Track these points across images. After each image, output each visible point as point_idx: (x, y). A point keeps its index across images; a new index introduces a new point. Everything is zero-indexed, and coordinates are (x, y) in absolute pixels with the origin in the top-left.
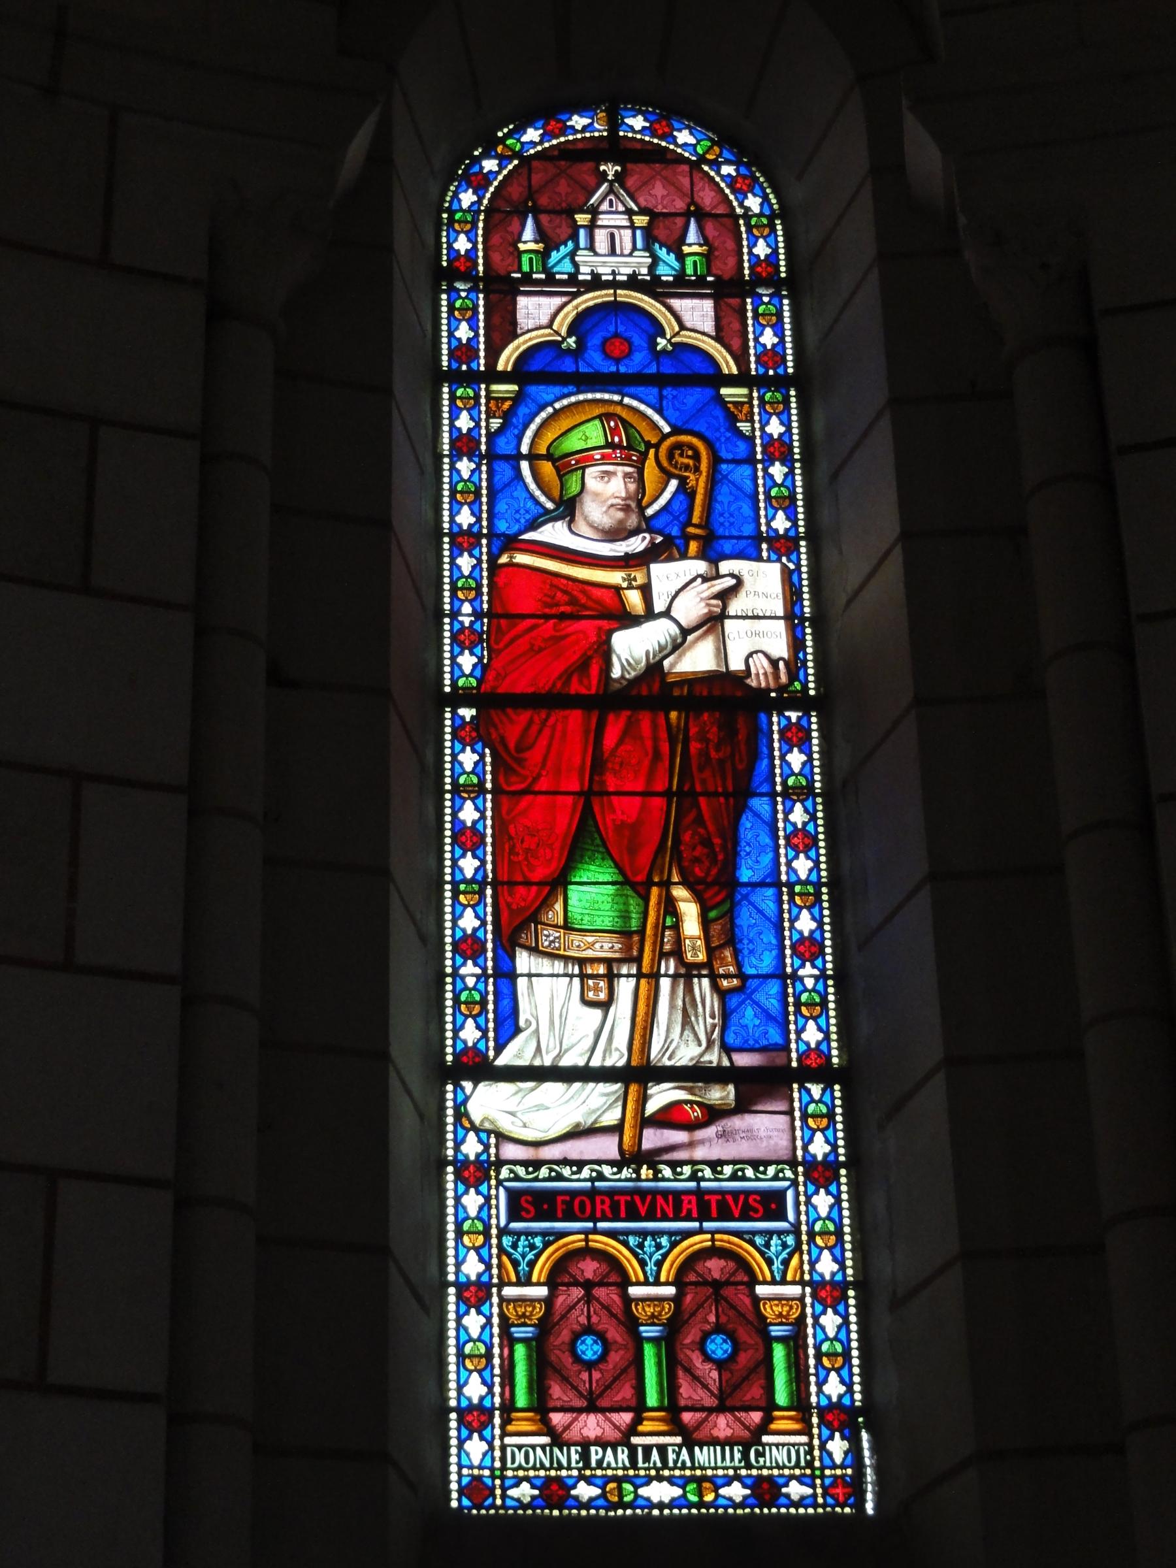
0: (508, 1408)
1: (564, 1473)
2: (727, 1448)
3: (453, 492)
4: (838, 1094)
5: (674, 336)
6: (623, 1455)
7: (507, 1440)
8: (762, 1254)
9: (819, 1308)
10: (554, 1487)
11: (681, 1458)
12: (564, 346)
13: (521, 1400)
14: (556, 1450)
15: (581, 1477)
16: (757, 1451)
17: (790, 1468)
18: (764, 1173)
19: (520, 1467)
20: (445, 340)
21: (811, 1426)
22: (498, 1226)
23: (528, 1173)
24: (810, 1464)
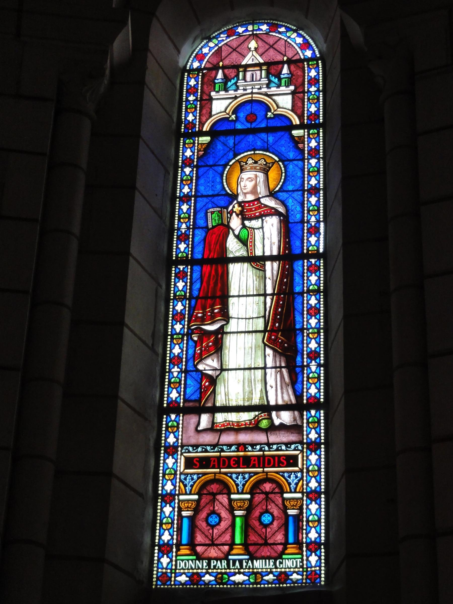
0: (179, 545)
1: (199, 571)
2: (267, 561)
3: (182, 180)
4: (322, 415)
5: (275, 111)
6: (224, 563)
7: (178, 558)
8: (287, 481)
9: (309, 501)
10: (195, 577)
11: (249, 565)
12: (230, 119)
13: (184, 541)
14: (197, 562)
15: (207, 573)
16: (280, 562)
17: (294, 568)
18: (290, 448)
19: (183, 569)
20: (185, 86)
21: (303, 551)
22: (180, 471)
23: (194, 450)
24: (302, 567)
